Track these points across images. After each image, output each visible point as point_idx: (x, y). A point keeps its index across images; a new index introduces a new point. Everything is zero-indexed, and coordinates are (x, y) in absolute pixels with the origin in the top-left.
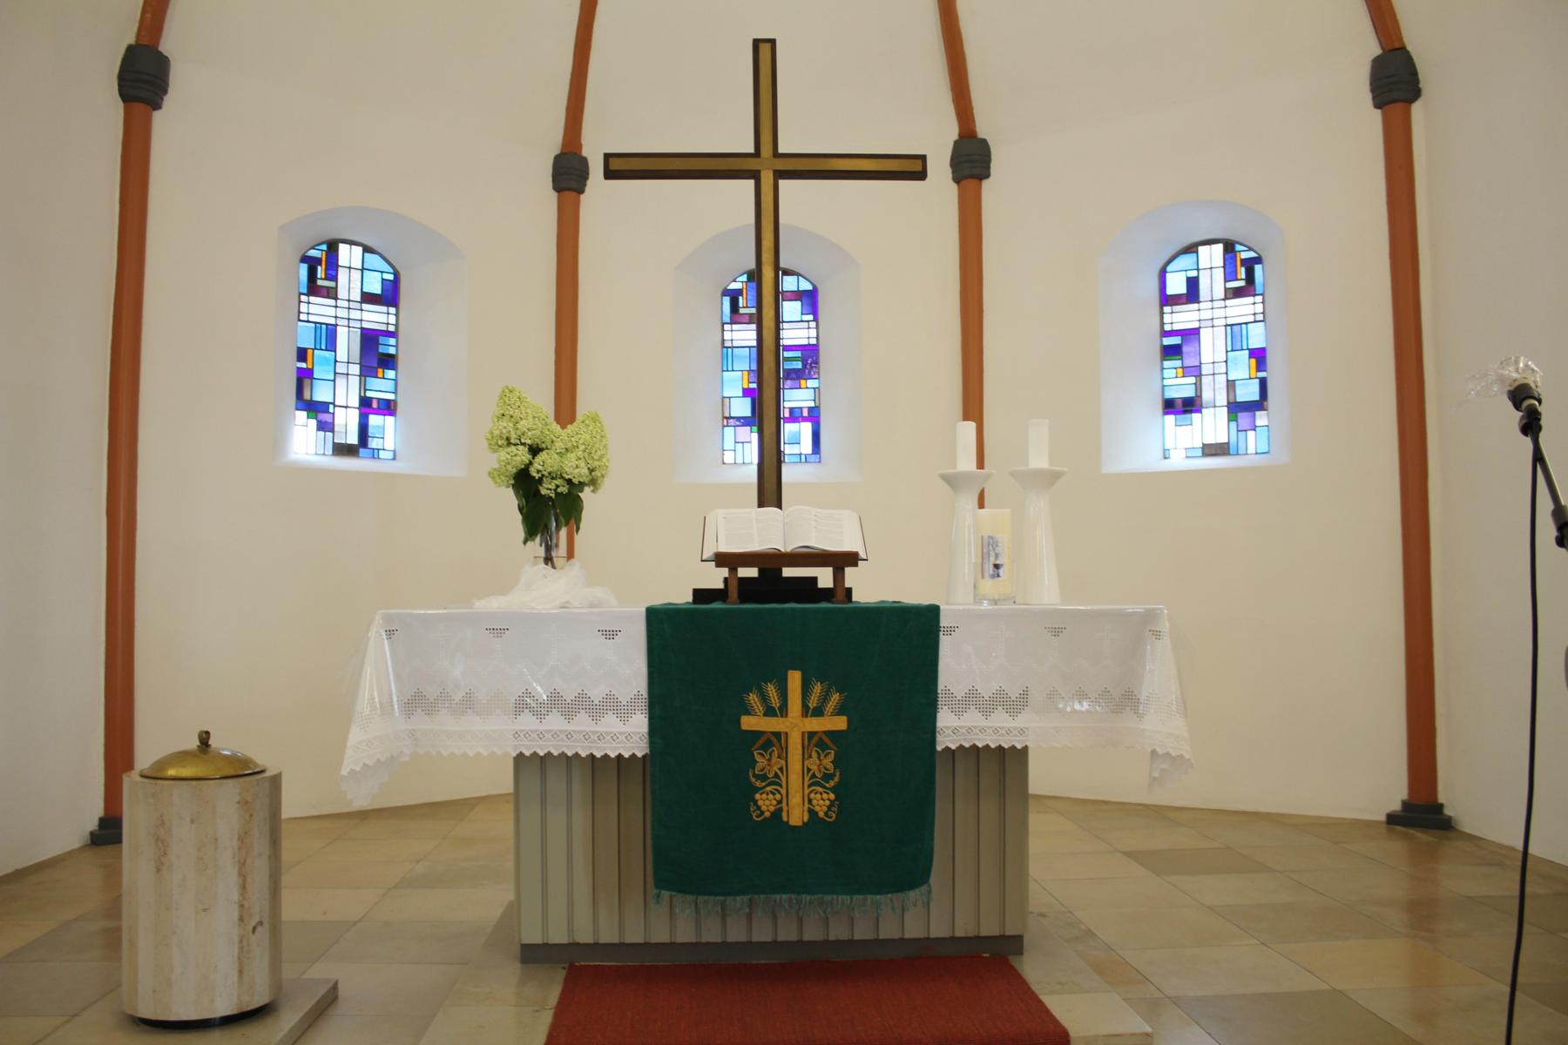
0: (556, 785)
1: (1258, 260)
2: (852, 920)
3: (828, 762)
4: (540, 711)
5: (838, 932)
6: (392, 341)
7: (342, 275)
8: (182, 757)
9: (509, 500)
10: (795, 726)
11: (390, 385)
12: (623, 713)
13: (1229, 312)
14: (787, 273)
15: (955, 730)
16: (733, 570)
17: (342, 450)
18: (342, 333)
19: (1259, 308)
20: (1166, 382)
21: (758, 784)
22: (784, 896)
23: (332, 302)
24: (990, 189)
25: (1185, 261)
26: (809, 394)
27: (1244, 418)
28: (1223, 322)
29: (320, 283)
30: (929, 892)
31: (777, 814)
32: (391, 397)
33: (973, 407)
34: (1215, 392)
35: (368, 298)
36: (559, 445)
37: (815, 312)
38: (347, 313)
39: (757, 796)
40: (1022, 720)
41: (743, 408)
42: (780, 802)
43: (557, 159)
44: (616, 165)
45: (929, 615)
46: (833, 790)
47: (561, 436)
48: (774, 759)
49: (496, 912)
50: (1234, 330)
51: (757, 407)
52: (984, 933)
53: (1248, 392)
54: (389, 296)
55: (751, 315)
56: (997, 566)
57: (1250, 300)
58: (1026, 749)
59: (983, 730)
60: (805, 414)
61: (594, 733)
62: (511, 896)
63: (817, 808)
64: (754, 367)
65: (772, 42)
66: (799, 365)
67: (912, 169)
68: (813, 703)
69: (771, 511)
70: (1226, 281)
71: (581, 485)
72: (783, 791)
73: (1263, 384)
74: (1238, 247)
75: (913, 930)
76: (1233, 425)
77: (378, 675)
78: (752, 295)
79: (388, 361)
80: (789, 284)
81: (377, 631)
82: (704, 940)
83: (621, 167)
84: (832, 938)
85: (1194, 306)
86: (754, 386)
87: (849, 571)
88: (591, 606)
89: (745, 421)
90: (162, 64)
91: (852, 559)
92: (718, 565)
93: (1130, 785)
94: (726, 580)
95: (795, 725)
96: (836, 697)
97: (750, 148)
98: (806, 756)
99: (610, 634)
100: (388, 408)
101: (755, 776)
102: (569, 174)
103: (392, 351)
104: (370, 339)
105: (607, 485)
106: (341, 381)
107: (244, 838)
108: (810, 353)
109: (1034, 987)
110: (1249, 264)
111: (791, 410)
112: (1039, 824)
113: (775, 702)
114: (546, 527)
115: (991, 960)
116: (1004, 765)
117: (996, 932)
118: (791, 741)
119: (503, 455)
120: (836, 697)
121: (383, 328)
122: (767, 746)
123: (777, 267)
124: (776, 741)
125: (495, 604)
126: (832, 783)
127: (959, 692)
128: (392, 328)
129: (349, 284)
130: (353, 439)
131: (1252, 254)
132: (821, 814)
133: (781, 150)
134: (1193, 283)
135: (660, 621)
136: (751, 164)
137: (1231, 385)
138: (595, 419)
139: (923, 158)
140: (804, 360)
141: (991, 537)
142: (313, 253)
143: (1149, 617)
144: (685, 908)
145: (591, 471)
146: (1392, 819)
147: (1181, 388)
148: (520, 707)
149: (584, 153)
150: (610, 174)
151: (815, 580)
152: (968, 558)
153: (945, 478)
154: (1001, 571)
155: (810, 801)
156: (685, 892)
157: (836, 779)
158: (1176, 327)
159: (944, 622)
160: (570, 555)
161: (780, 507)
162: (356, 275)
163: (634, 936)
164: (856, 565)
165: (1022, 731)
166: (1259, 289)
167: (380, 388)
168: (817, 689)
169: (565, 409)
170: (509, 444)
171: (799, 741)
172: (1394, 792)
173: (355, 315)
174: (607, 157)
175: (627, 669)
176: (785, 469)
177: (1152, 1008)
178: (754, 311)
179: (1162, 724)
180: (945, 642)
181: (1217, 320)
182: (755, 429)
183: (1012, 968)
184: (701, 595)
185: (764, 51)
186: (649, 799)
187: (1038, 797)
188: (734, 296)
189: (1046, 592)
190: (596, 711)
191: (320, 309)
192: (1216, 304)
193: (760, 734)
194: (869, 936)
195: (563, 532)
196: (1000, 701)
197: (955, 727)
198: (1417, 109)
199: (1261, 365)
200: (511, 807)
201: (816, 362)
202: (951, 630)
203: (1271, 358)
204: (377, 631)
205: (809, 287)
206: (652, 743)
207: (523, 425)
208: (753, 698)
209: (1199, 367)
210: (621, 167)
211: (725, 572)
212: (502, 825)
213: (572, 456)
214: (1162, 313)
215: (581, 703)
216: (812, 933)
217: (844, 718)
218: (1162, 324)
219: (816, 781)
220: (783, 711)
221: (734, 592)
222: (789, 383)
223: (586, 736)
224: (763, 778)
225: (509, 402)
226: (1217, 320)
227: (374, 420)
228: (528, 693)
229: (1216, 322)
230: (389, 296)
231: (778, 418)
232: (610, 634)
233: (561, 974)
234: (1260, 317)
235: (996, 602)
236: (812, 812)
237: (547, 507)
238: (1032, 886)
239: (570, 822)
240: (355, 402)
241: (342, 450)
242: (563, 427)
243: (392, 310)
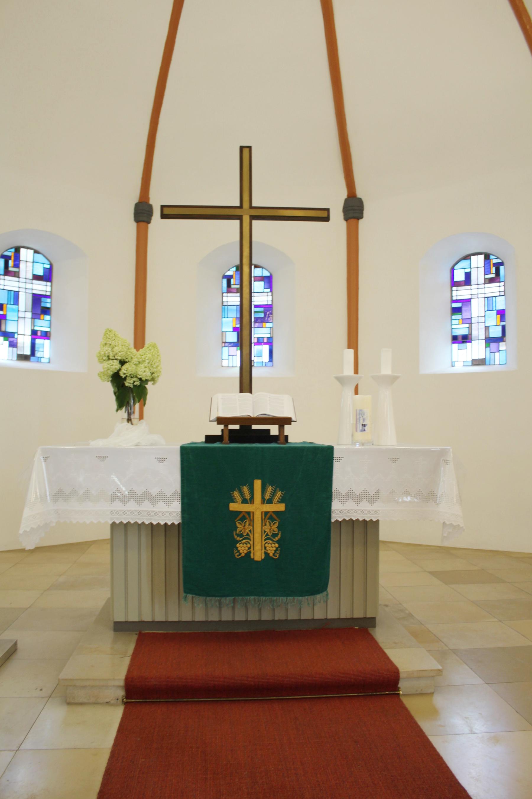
0: (133, 538)
1: (502, 264)
2: (287, 610)
3: (275, 527)
4: (124, 500)
5: (280, 616)
6: (49, 300)
7: (22, 265)
9: (109, 389)
10: (258, 508)
11: (47, 324)
12: (168, 501)
13: (487, 290)
14: (256, 267)
15: (341, 511)
16: (226, 426)
17: (23, 358)
19: (502, 289)
20: (453, 327)
21: (238, 539)
22: (252, 597)
23: (17, 279)
24: (364, 225)
25: (464, 264)
26: (267, 330)
27: (493, 345)
28: (483, 296)
29: (11, 269)
30: (327, 595)
31: (248, 554)
32: (47, 330)
33: (353, 341)
34: (478, 332)
35: (36, 277)
36: (135, 360)
37: (271, 287)
38: (26, 286)
39: (238, 545)
40: (376, 506)
41: (233, 337)
42: (249, 548)
43: (137, 205)
44: (167, 211)
45: (329, 450)
46: (277, 542)
47: (136, 355)
48: (246, 527)
49: (101, 604)
51: (240, 337)
52: (355, 616)
53: (496, 332)
55: (237, 289)
56: (364, 426)
57: (497, 284)
58: (378, 521)
59: (355, 511)
60: (265, 341)
61: (153, 511)
62: (109, 595)
63: (269, 552)
64: (238, 316)
65: (250, 148)
66: (262, 315)
67: (322, 216)
68: (267, 497)
69: (246, 395)
70: (485, 275)
71: (147, 381)
72: (251, 542)
73: (504, 328)
74: (492, 257)
75: (319, 614)
76: (488, 349)
77: (39, 481)
78: (238, 277)
79: (46, 311)
80: (257, 272)
81: (39, 458)
82: (209, 620)
83: (170, 213)
84: (276, 618)
85: (468, 287)
86: (238, 326)
87: (286, 427)
88: (152, 445)
89: (234, 344)
91: (288, 421)
92: (218, 423)
93: (432, 537)
94: (222, 430)
95: (258, 508)
96: (279, 494)
97: (238, 204)
98: (263, 524)
99: (162, 460)
100: (46, 336)
101: (236, 534)
102: (142, 213)
103: (48, 305)
104: (37, 299)
105: (160, 381)
106: (21, 321)
108: (268, 308)
109: (382, 645)
110: (497, 266)
111: (258, 339)
112: (383, 555)
113: (247, 496)
114: (128, 403)
115: (359, 631)
116: (366, 530)
117: (361, 616)
118: (255, 516)
119: (106, 365)
120: (279, 494)
121: (44, 293)
122: (243, 519)
123: (251, 264)
124: (247, 516)
125: (99, 443)
126: (277, 539)
128: (48, 294)
130: (28, 352)
131: (499, 261)
132: (271, 555)
133: (254, 205)
134: (468, 276)
135: (188, 453)
136: (238, 212)
137: (487, 328)
138: (154, 346)
139: (328, 210)
141: (361, 410)
142: (6, 253)
143: (443, 453)
144: (200, 603)
145: (152, 374)
147: (462, 330)
148: (114, 497)
149: (151, 202)
150: (164, 216)
151: (268, 431)
152: (349, 420)
153: (338, 379)
154: (366, 428)
155: (265, 548)
156: (200, 595)
157: (279, 536)
158: (459, 298)
159: (336, 455)
160: (141, 417)
161: (251, 392)
162: (30, 265)
163: (173, 618)
164: (290, 424)
165: (376, 512)
166: (502, 279)
167: (42, 325)
168: (270, 489)
169: (139, 340)
170: (109, 359)
171: (260, 516)
173: (29, 286)
174: (162, 207)
175: (170, 478)
176: (254, 370)
177: (442, 655)
178: (238, 286)
179: (449, 509)
180: (336, 466)
181: (481, 295)
182: (239, 348)
183: (370, 635)
184: (210, 439)
185: (245, 152)
186: (181, 537)
187: (384, 542)
188: (229, 279)
189: (390, 440)
190: (153, 500)
191: (10, 283)
192: (480, 286)
193: (238, 513)
194: (296, 617)
195: (137, 406)
196: (365, 496)
197: (341, 510)
200: (109, 546)
201: (271, 314)
202: (340, 459)
204: (39, 458)
205: (268, 274)
206: (183, 517)
207: (116, 349)
208: (236, 494)
209: (471, 319)
210: (170, 213)
211: (222, 427)
212: (104, 556)
213: (142, 366)
214: (452, 291)
215: (146, 496)
216: (266, 616)
217: (283, 505)
218: (452, 296)
220: (252, 500)
221: (226, 437)
222: (257, 324)
223: (149, 513)
224: (241, 535)
225: (109, 337)
226: (481, 295)
227: (38, 341)
228: (119, 491)
229: (480, 296)
231: (251, 343)
233: (134, 638)
234: (502, 293)
235: (363, 444)
236: (266, 554)
237: (129, 393)
238: (381, 590)
239: (140, 557)
240: (30, 333)
241: (23, 358)
242: (138, 350)
243: (49, 284)
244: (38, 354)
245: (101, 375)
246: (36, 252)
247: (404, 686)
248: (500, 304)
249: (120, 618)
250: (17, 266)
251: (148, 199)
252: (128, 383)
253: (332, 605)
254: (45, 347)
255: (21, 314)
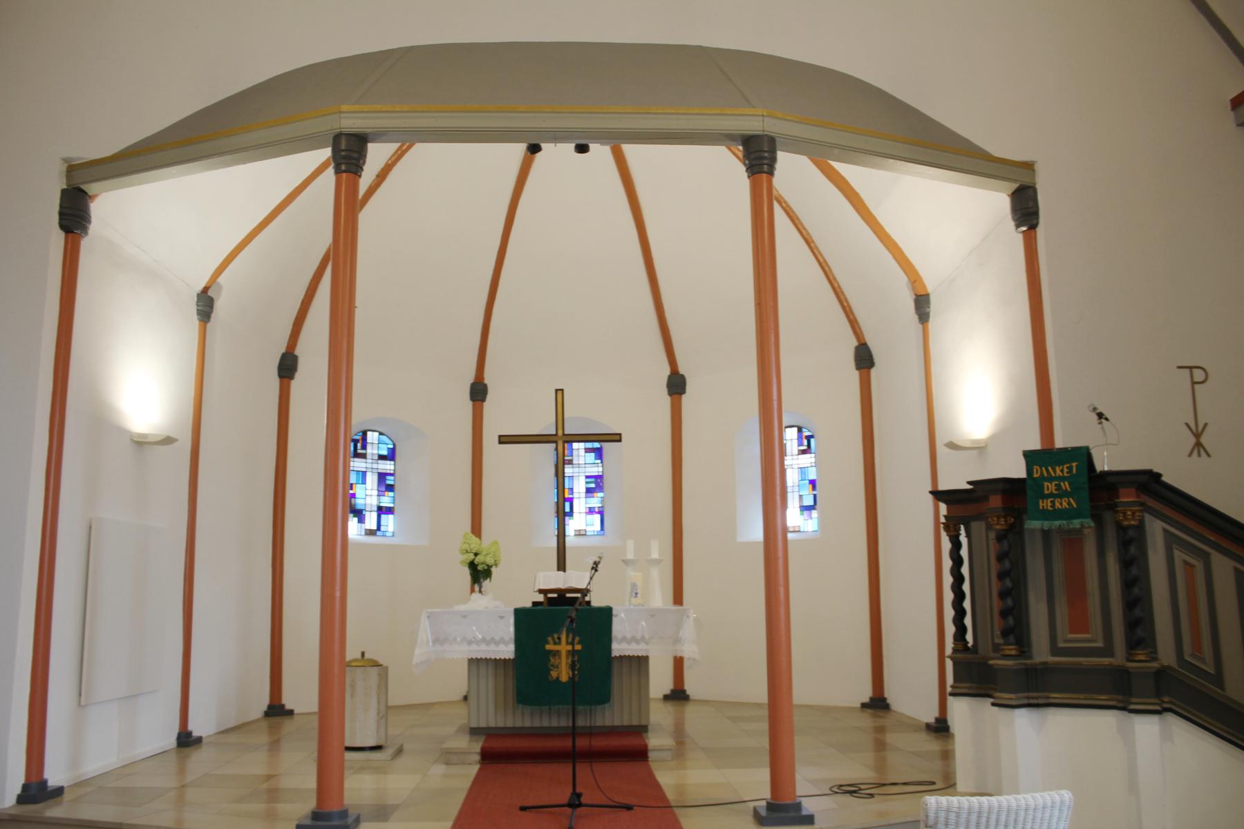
1: (812, 436)
4: (478, 642)
7: (369, 447)
8: (355, 660)
9: (466, 572)
10: (562, 647)
12: (506, 643)
17: (370, 533)
18: (369, 476)
35: (382, 457)
43: (472, 385)
50: (802, 470)
54: (391, 456)
73: (815, 496)
77: (425, 631)
79: (390, 488)
81: (424, 619)
90: (295, 359)
96: (577, 639)
100: (389, 511)
104: (382, 476)
105: (500, 566)
107: (379, 686)
110: (809, 438)
120: (577, 639)
124: (556, 654)
125: (462, 608)
127: (619, 636)
129: (371, 451)
135: (520, 614)
137: (801, 496)
140: (596, 483)
146: (864, 706)
159: (614, 612)
172: (866, 694)
173: (375, 466)
180: (615, 620)
184: (535, 604)
190: (497, 643)
191: (357, 464)
193: (550, 651)
196: (634, 639)
197: (618, 649)
198: (873, 371)
199: (814, 488)
203: (818, 484)
204: (424, 619)
219: (573, 666)
220: (560, 643)
230: (391, 456)
232: (502, 617)
239: (488, 684)
244: (383, 528)
245: (462, 562)
246: (381, 434)
247: (651, 755)
248: (812, 475)
249: (474, 725)
250: (364, 447)
251: (483, 378)
252: (480, 568)
253: (612, 716)
254: (389, 521)
255: (368, 492)
